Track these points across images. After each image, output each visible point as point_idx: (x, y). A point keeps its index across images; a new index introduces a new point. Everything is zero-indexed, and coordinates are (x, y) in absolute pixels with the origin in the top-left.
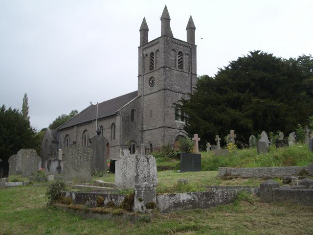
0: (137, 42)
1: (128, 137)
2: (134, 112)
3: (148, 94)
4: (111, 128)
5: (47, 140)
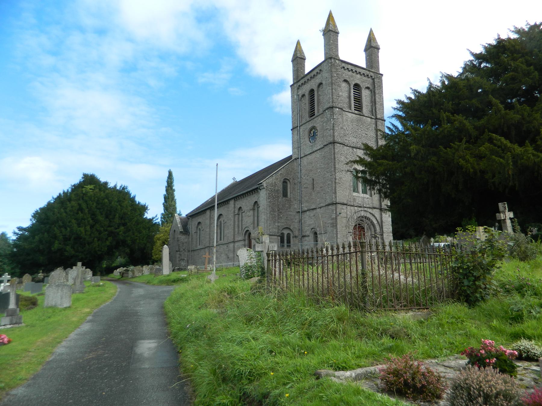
1: (278, 222)
2: (286, 183)
3: (307, 154)
4: (254, 209)
5: (175, 230)
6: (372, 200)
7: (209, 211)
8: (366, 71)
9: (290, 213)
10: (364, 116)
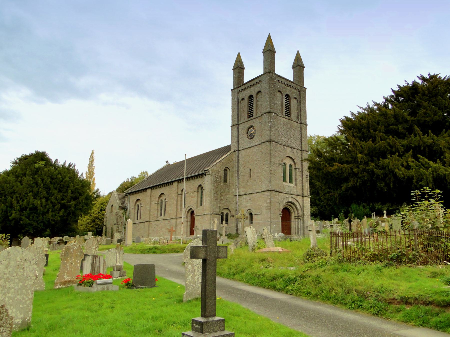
0: (230, 83)
1: (220, 203)
2: (227, 171)
4: (198, 191)
6: (297, 189)
7: (150, 189)
8: (295, 85)
9: (229, 196)
10: (292, 121)
